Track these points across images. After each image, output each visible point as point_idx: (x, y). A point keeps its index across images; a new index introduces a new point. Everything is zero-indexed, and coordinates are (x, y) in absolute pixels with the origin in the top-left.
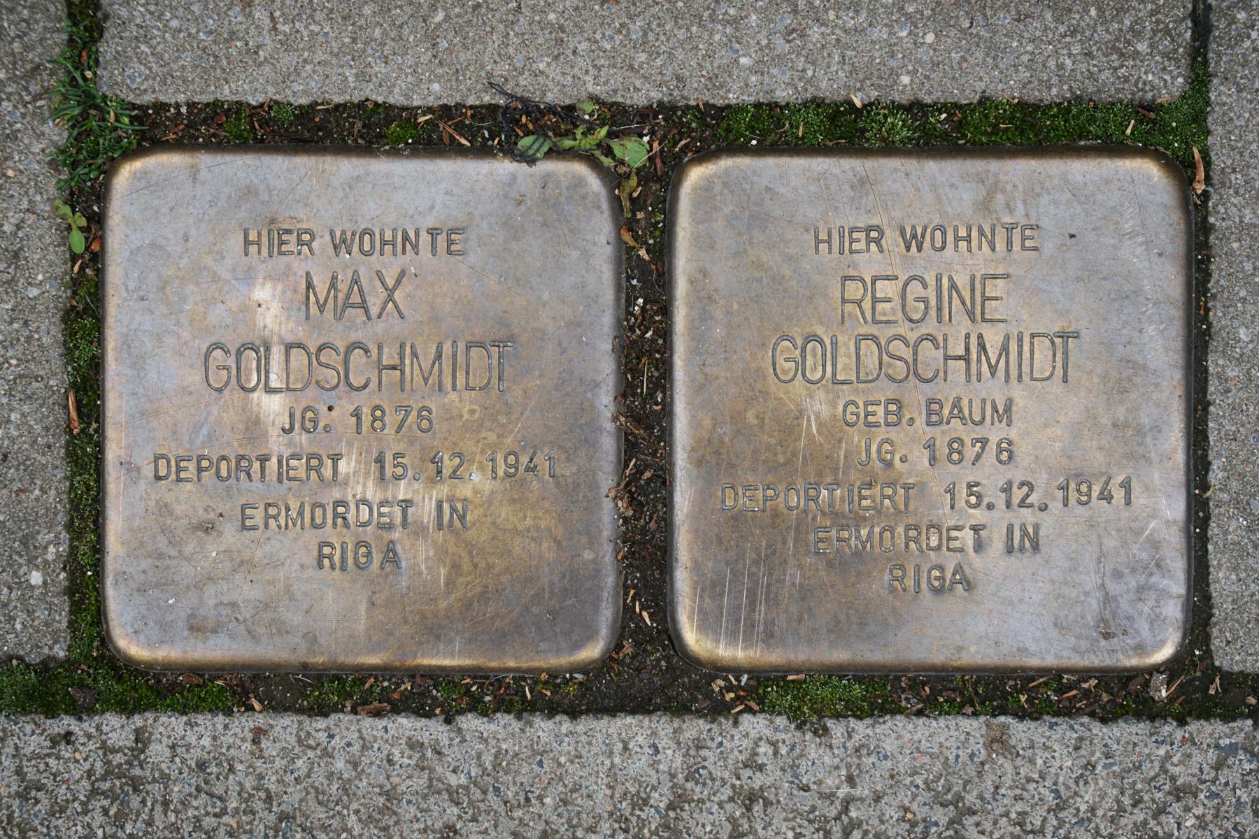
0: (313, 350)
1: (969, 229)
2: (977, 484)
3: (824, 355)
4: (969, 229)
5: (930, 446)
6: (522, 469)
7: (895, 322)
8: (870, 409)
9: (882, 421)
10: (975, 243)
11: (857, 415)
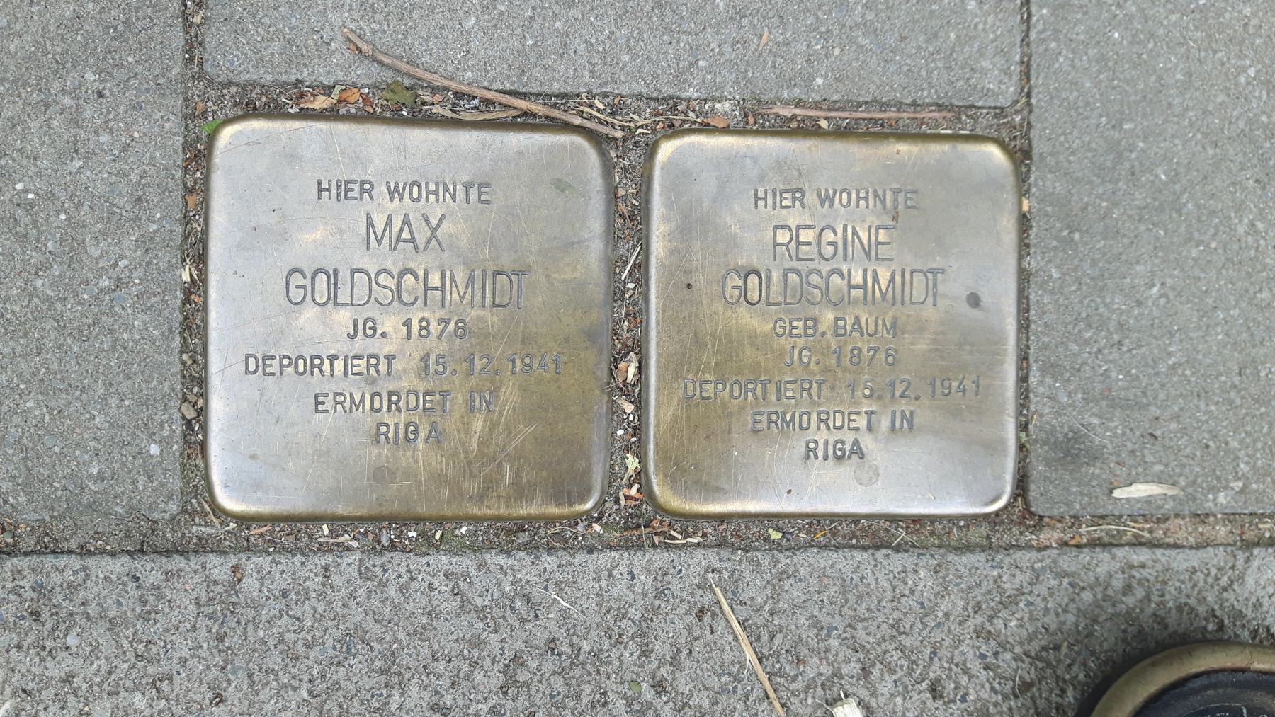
3: (760, 284)
11: (784, 328)
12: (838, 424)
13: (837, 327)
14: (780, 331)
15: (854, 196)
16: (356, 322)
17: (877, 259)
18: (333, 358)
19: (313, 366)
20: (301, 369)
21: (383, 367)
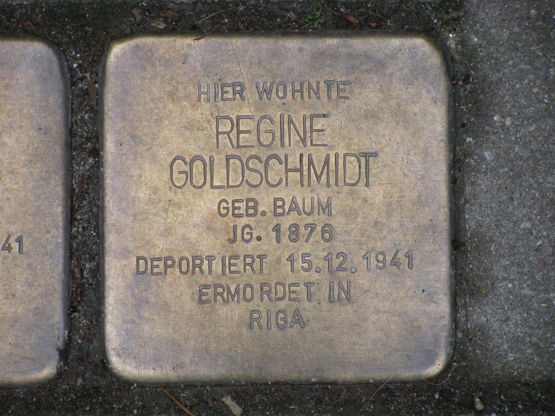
0: (188, 160)
1: (302, 84)
2: (309, 255)
3: (205, 169)
4: (302, 84)
5: (277, 229)
6: (388, 263)
7: (253, 146)
8: (236, 205)
9: (245, 214)
10: (306, 94)
11: (227, 209)
12: (280, 295)
13: (276, 207)
14: (223, 212)
15: (289, 88)
16: (235, 227)
17: (312, 145)
18: (211, 258)
19: (194, 266)
20: (184, 269)
21: (205, 267)
